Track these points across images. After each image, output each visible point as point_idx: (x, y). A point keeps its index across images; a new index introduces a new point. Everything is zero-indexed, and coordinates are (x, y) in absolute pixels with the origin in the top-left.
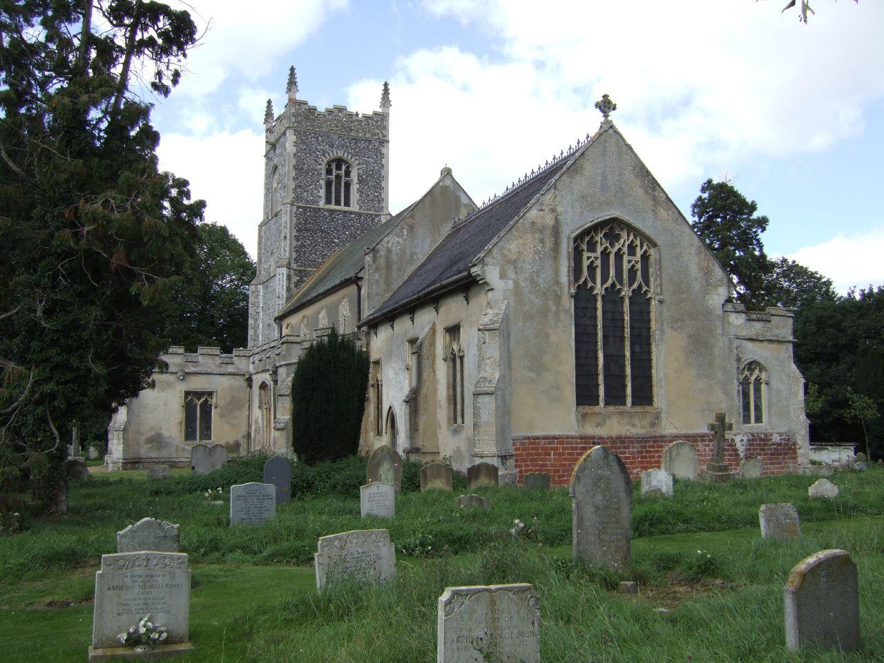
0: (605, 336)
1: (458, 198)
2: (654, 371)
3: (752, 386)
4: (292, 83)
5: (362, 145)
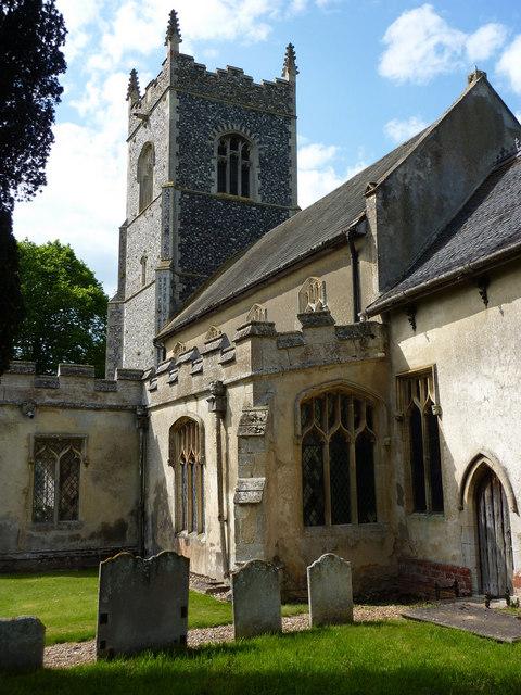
1: (498, 118)
5: (264, 119)
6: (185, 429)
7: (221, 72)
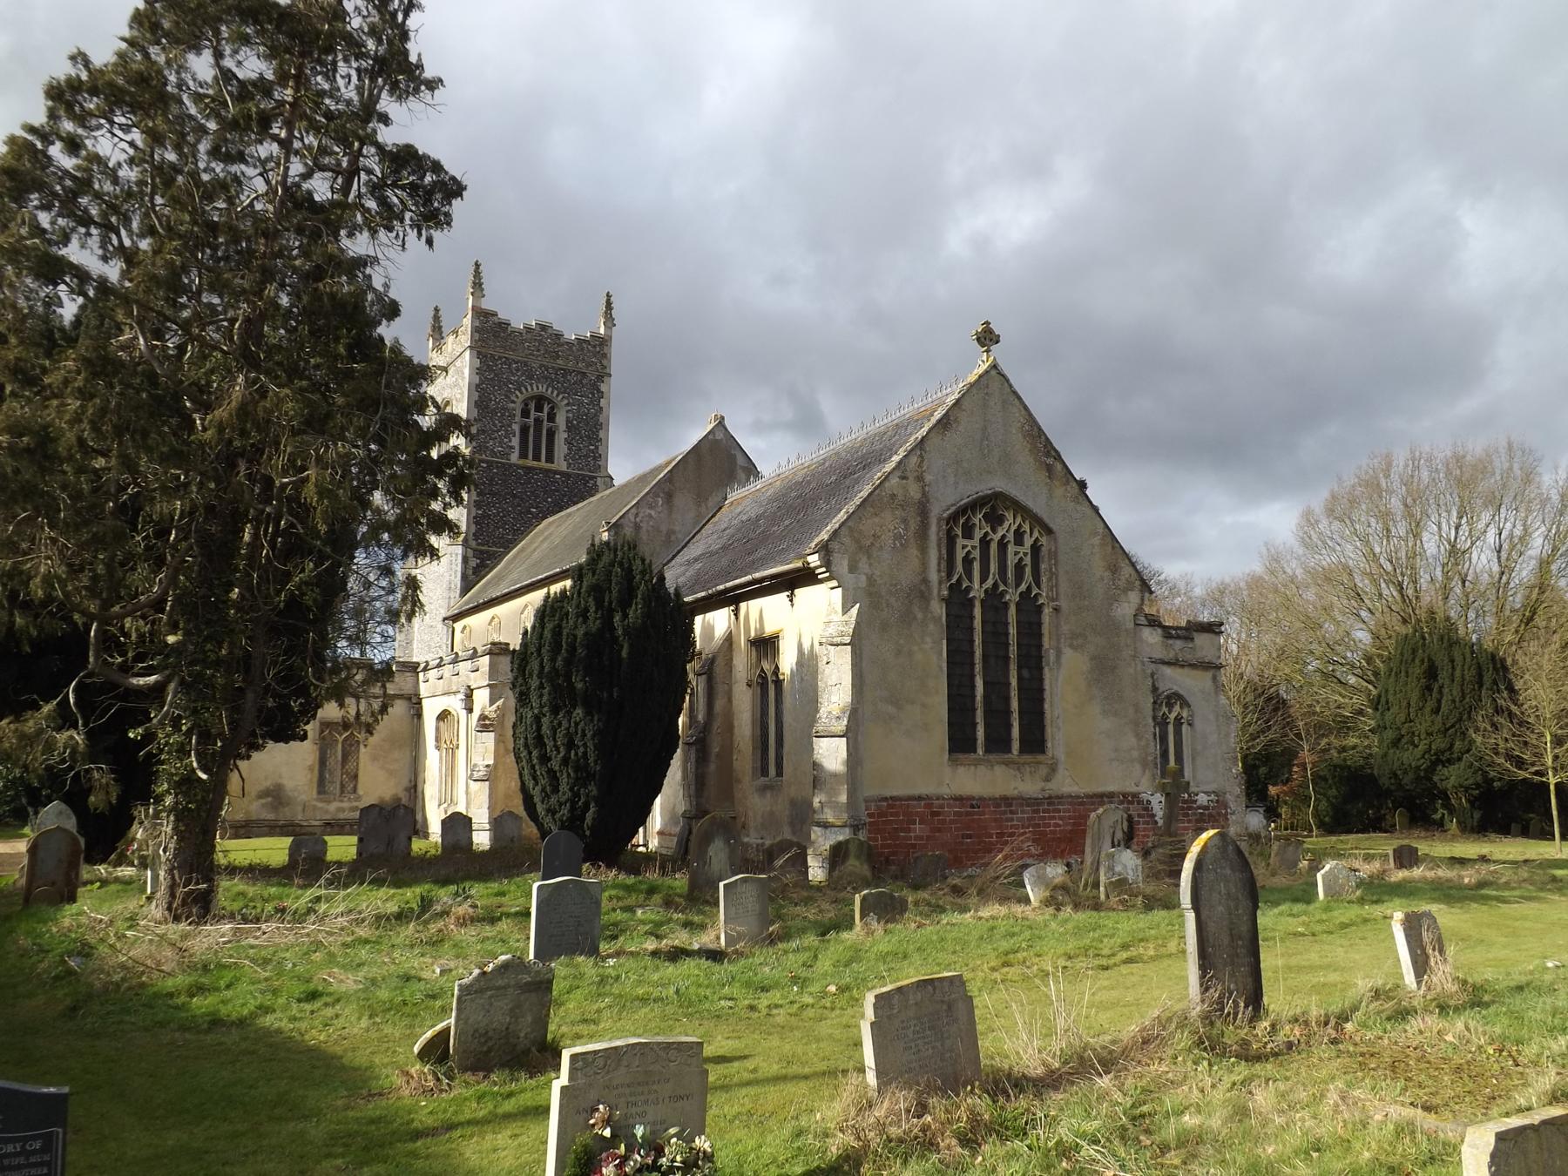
0: (985, 657)
1: (733, 459)
2: (1047, 706)
3: (1171, 728)
4: (478, 285)
5: (573, 378)
6: (444, 716)
7: (528, 329)
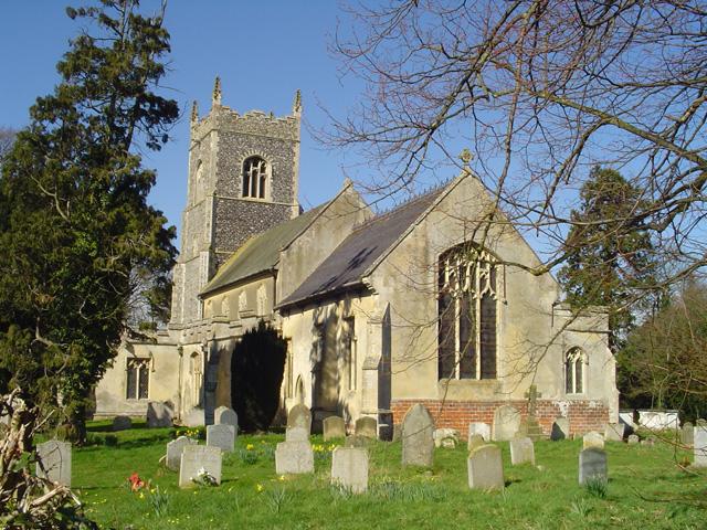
3: (574, 366)
5: (277, 145)
